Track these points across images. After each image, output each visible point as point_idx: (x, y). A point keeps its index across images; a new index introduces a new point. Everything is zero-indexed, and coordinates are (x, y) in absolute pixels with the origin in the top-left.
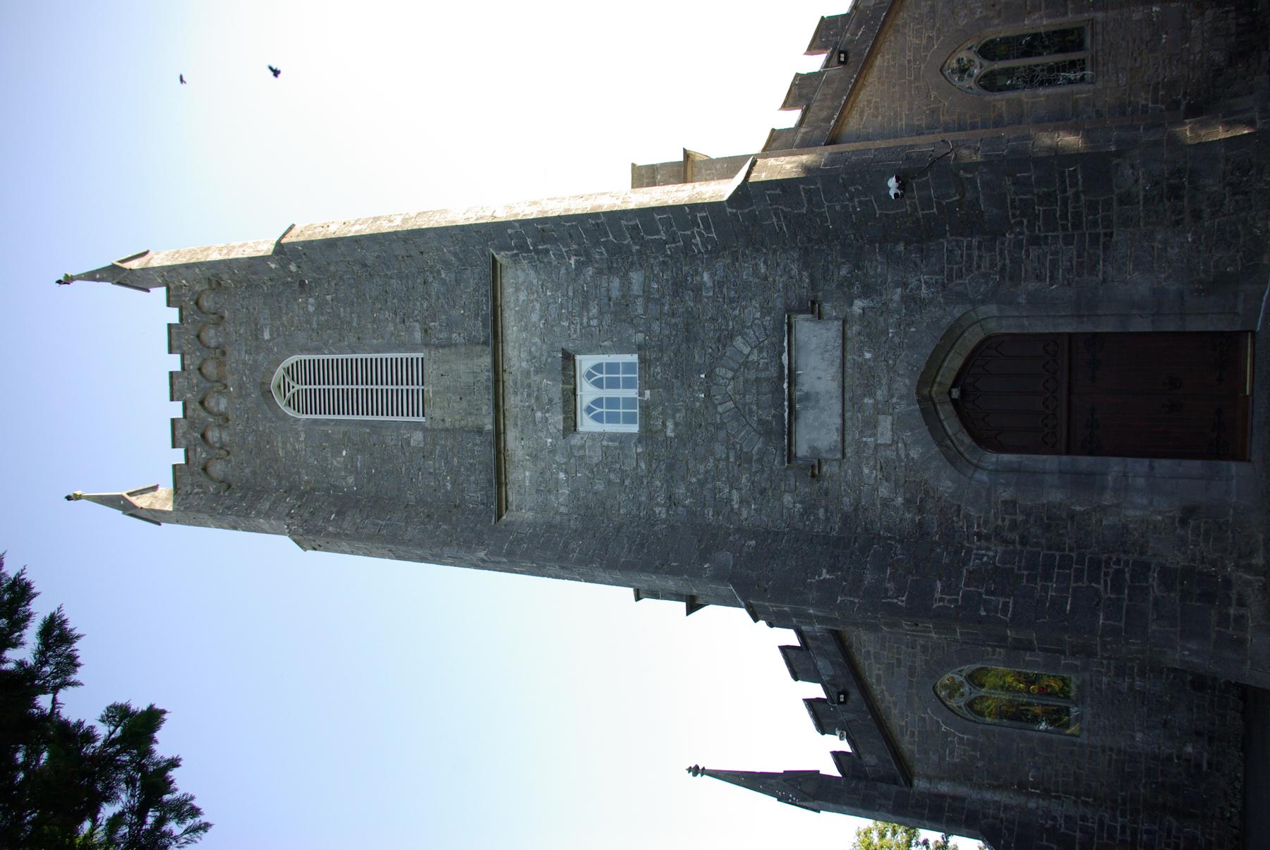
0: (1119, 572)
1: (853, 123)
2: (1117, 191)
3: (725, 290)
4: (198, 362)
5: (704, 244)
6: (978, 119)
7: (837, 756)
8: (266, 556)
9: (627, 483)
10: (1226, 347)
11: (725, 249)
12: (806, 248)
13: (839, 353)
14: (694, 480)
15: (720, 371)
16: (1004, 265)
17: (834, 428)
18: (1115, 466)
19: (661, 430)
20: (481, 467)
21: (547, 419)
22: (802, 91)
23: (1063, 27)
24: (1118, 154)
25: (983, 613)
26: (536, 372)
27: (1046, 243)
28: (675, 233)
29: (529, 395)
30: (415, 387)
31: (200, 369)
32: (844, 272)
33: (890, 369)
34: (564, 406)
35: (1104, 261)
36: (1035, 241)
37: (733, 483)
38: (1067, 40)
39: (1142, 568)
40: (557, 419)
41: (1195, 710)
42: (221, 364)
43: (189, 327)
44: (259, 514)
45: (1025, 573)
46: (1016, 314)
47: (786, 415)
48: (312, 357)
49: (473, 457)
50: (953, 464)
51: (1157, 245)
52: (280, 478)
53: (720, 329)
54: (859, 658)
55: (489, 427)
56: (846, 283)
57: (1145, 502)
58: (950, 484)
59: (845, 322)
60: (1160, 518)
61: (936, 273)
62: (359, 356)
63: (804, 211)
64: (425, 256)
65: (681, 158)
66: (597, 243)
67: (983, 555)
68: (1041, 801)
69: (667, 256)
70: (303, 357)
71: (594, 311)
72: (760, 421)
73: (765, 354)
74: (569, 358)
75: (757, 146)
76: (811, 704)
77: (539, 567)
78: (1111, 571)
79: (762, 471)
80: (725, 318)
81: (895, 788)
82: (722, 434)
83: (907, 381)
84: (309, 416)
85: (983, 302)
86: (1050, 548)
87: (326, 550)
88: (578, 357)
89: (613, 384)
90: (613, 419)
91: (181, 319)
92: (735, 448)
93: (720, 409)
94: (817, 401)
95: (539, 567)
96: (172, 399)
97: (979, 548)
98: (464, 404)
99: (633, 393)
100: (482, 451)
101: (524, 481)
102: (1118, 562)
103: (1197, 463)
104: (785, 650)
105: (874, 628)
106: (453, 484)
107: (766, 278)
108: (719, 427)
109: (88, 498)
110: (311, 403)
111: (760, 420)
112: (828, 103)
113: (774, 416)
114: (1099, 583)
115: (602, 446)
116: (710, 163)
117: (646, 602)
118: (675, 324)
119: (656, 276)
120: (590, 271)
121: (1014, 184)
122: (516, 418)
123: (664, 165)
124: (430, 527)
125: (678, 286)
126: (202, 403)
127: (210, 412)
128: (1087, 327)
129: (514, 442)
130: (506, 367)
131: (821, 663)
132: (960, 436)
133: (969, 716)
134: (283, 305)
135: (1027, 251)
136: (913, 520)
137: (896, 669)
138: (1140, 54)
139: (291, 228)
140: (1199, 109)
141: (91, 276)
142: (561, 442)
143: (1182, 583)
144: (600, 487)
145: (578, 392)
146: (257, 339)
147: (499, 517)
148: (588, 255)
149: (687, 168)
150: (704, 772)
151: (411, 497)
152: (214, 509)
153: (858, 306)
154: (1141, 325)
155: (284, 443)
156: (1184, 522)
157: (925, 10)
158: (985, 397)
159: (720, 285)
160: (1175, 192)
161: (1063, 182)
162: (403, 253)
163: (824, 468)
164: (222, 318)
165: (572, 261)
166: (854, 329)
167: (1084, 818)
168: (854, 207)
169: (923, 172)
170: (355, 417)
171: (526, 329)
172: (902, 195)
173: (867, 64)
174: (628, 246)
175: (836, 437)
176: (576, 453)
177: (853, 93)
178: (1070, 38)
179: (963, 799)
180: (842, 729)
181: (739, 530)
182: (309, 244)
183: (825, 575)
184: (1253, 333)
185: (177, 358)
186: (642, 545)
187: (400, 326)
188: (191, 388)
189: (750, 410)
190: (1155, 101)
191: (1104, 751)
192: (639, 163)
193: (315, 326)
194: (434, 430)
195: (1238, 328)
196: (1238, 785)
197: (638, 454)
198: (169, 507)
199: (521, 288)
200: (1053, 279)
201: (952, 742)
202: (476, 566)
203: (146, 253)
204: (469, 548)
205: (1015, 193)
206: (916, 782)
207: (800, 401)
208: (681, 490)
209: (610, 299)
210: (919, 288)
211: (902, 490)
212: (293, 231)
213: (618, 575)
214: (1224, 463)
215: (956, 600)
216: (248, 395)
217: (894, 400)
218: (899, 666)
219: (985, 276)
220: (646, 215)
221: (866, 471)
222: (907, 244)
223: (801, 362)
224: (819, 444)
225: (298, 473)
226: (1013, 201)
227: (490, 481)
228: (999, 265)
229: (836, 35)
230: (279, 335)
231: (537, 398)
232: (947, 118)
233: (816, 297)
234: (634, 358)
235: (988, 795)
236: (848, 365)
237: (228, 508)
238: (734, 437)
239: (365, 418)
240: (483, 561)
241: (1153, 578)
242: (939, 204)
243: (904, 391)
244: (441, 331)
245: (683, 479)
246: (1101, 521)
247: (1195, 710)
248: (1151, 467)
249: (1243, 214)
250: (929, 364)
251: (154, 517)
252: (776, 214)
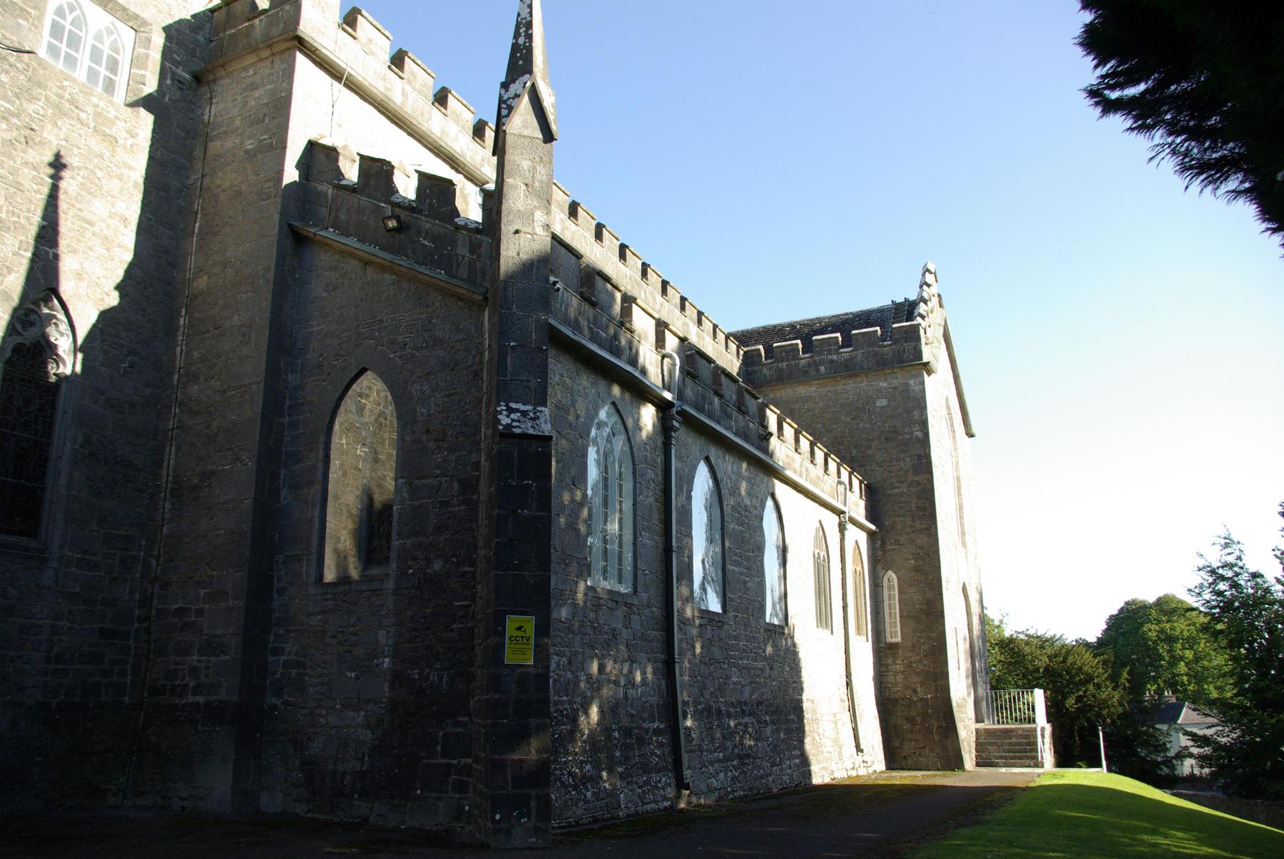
138: (340, 643)
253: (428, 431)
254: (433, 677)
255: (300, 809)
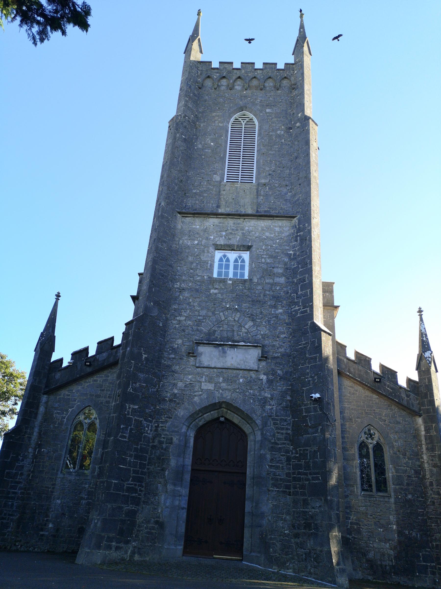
0: (135, 491)
1: (347, 383)
2: (309, 498)
3: (274, 319)
4: (258, 77)
5: (295, 311)
6: (346, 440)
7: (61, 360)
8: (168, 104)
9: (191, 271)
10: (235, 546)
11: (292, 320)
12: (291, 356)
13: (243, 367)
14: (191, 300)
15: (238, 315)
16: (279, 444)
17: (210, 363)
18: (185, 491)
19: (214, 287)
20: (202, 206)
21: (222, 237)
22: (363, 361)
23: (388, 482)
24: (326, 500)
25: (122, 426)
26: (243, 233)
27: (287, 464)
28: (301, 298)
29: (233, 230)
30: (240, 179)
31: (255, 77)
32: (279, 372)
33: (235, 390)
34: (227, 245)
35: (278, 491)
36: (288, 459)
37: (188, 318)
38: (382, 485)
39: (137, 502)
40: (222, 242)
41: (68, 529)
42: (256, 88)
43: (275, 73)
44: (186, 101)
45: (139, 447)
46: (256, 449)
47: (217, 343)
48: (257, 131)
49: (207, 203)
50: (190, 416)
51: (284, 516)
52: (203, 113)
53: (257, 315)
54: (106, 372)
55: (220, 211)
56: (274, 373)
57: (168, 504)
58: (181, 414)
59: (257, 371)
60: (160, 511)
61: (276, 413)
62: (256, 154)
63: (307, 356)
64: (299, 186)
65: (336, 304)
66: (298, 263)
67: (148, 428)
68: (32, 454)
69: (291, 294)
70: (257, 127)
71: (268, 261)
72: (215, 331)
73: (244, 335)
74: (248, 248)
75: (339, 339)
76: (86, 350)
77: (156, 229)
78: (137, 487)
79: (193, 331)
80: (262, 318)
81: (43, 386)
82: (210, 314)
83: (229, 397)
84: (230, 129)
85: (262, 434)
86: (149, 459)
87: (169, 132)
88: (248, 252)
89: (236, 267)
90: (220, 266)
91: (278, 70)
92: (204, 319)
93: (221, 314)
94: (222, 357)
95: (156, 229)
96: (242, 63)
97: (152, 426)
98: (231, 200)
99: (231, 276)
100: (210, 207)
101: (195, 225)
102: (141, 491)
103: (183, 530)
104: (112, 339)
105: (119, 377)
106: (196, 193)
107: (278, 337)
108: (213, 313)
109: (198, 19)
110: (236, 131)
111: (215, 331)
112: (357, 372)
113: (217, 337)
114: (132, 481)
115: (208, 261)
116: (333, 318)
117: (138, 278)
118: (260, 296)
119: (282, 289)
120: (286, 260)
121: (315, 451)
122: (223, 223)
123: (333, 297)
124: (176, 181)
125: (277, 298)
126: (239, 77)
127: (235, 81)
128: (248, 482)
129: (212, 222)
130: (246, 220)
131: (105, 355)
132: (203, 420)
133: (75, 421)
134: (281, 119)
135: (284, 455)
136: (166, 397)
137: (99, 389)
138: (374, 518)
139: (316, 124)
140: (345, 543)
141: (302, 27)
142: (211, 243)
143: (128, 520)
144: (190, 259)
145: (233, 252)
146: (267, 106)
147: (180, 213)
148: (294, 259)
149: (330, 306)
150: (57, 299)
151: (190, 174)
152: (190, 80)
153: (264, 377)
154: (248, 507)
155: (218, 116)
156: (157, 522)
157: (398, 419)
158: (220, 432)
159: (276, 317)
160: (308, 526)
161: (315, 474)
162: (301, 176)
163: (192, 358)
164: (278, 90)
165: (291, 252)
166: (253, 375)
167: (22, 474)
168: (307, 378)
169: (321, 409)
170: (228, 150)
171: (263, 230)
172: (312, 400)
173: (374, 391)
174: (296, 277)
175: (206, 364)
176: (206, 249)
177: (361, 383)
178: (383, 485)
179: (35, 417)
180: (74, 363)
181: (167, 319)
182: (308, 132)
183: (144, 356)
184: (242, 560)
185: (260, 66)
186: (163, 276)
187: (268, 173)
188: (246, 72)
189: (220, 327)
190: (352, 523)
191: (53, 485)
192: (334, 286)
193: (271, 134)
194: (220, 186)
195: (244, 553)
196: (31, 549)
197: (204, 276)
198: (192, 58)
199: (282, 228)
200: (271, 466)
201: (63, 413)
202: (157, 201)
203: (311, 55)
204: (166, 198)
205: (310, 452)
206: (45, 396)
207: (223, 349)
208: (186, 294)
209: (273, 268)
210: (270, 405)
211: (180, 392)
212: (315, 125)
213: (150, 264)
214: (183, 543)
215: (129, 415)
216: (241, 100)
217: (221, 391)
218: (101, 390)
219: (274, 435)
220: (310, 285)
221: (190, 377)
222: (290, 401)
223: (240, 350)
224: (203, 356)
225: (204, 122)
226: (307, 450)
227: (196, 210)
228: (279, 442)
229: (388, 378)
230: (268, 116)
231: (231, 233)
232: (347, 426)
233: (269, 359)
234: (246, 277)
235: (36, 430)
236: (238, 371)
237: (190, 87)
238: (208, 319)
239: (228, 155)
240: (160, 204)
241: (132, 507)
242: (306, 416)
243: (224, 396)
244: (264, 192)
245: (192, 296)
246: (160, 483)
247: (68, 529)
248: (183, 509)
249: (296, 558)
250: (236, 408)
251: (188, 51)
252: (306, 343)
253: (399, 451)
254: (414, 534)
255: (370, 578)
